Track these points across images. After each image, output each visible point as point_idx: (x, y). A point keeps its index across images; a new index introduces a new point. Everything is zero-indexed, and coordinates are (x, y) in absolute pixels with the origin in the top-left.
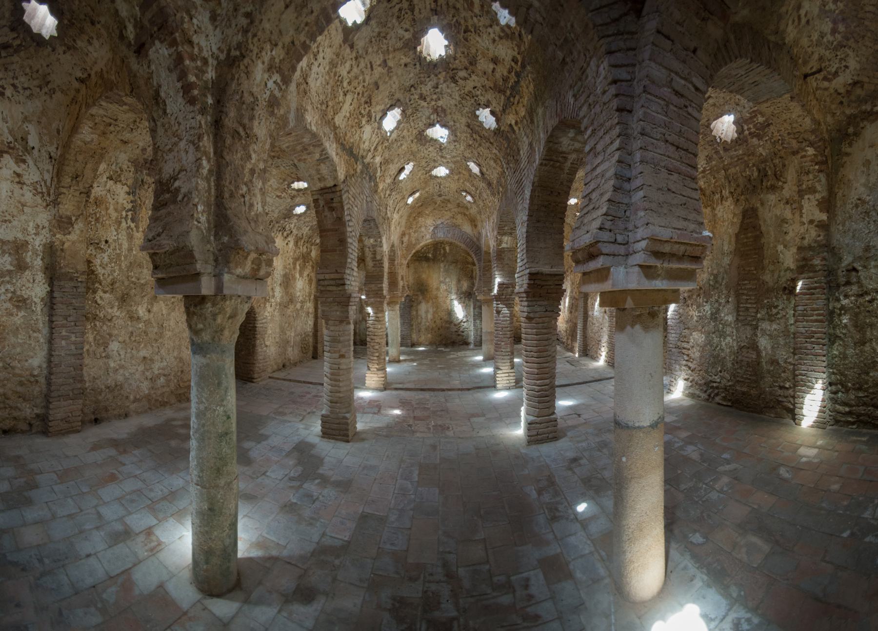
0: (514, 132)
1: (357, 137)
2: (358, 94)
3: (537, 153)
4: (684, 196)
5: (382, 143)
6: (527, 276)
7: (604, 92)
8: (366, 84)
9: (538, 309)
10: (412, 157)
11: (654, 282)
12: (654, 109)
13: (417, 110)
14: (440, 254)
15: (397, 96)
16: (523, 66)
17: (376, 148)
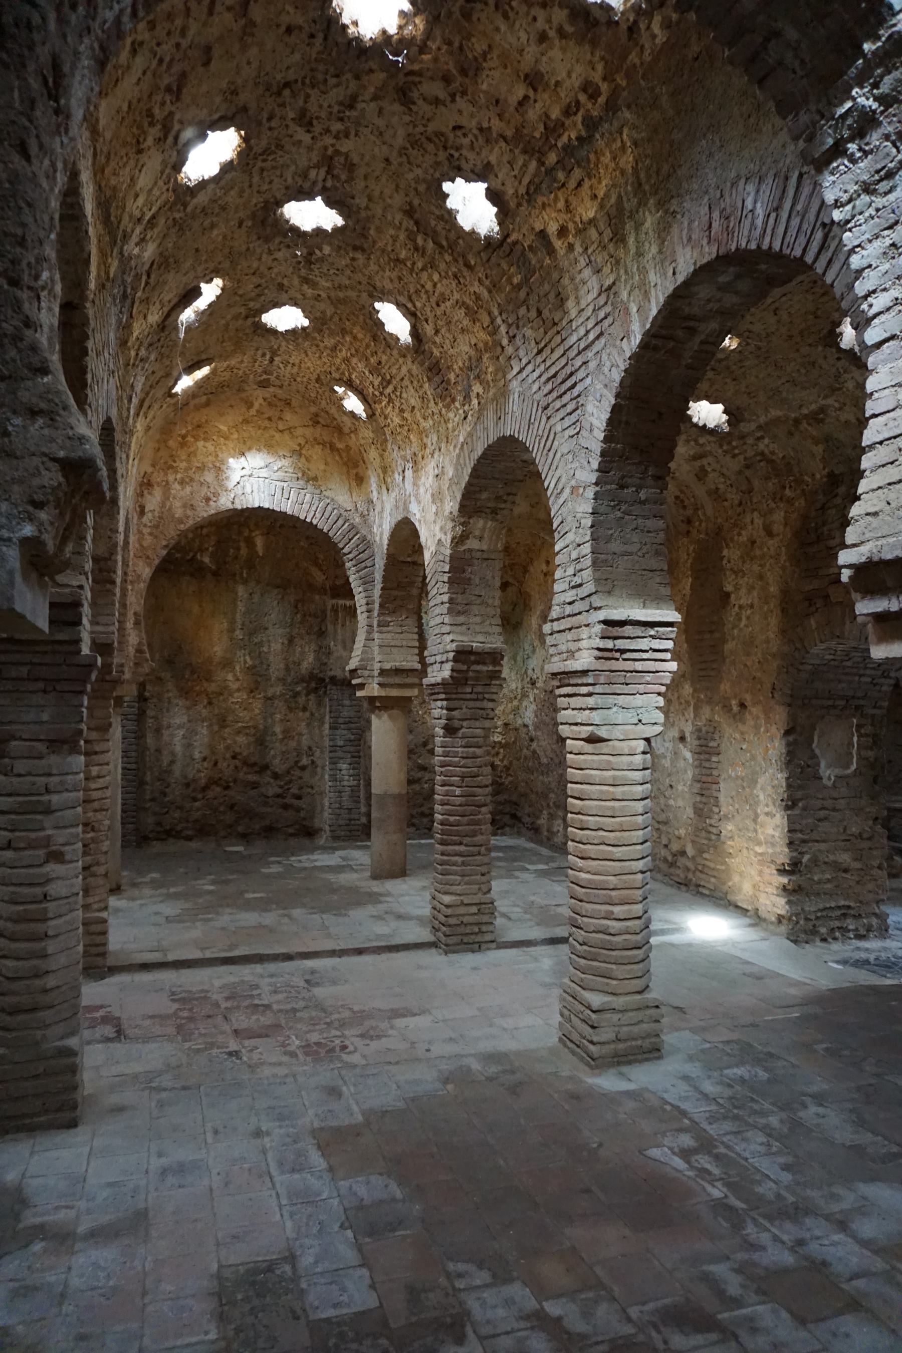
0: (551, 251)
2: (161, 61)
8: (184, 43)
10: (226, 265)
15: (244, 97)
16: (611, 107)
17: (153, 217)
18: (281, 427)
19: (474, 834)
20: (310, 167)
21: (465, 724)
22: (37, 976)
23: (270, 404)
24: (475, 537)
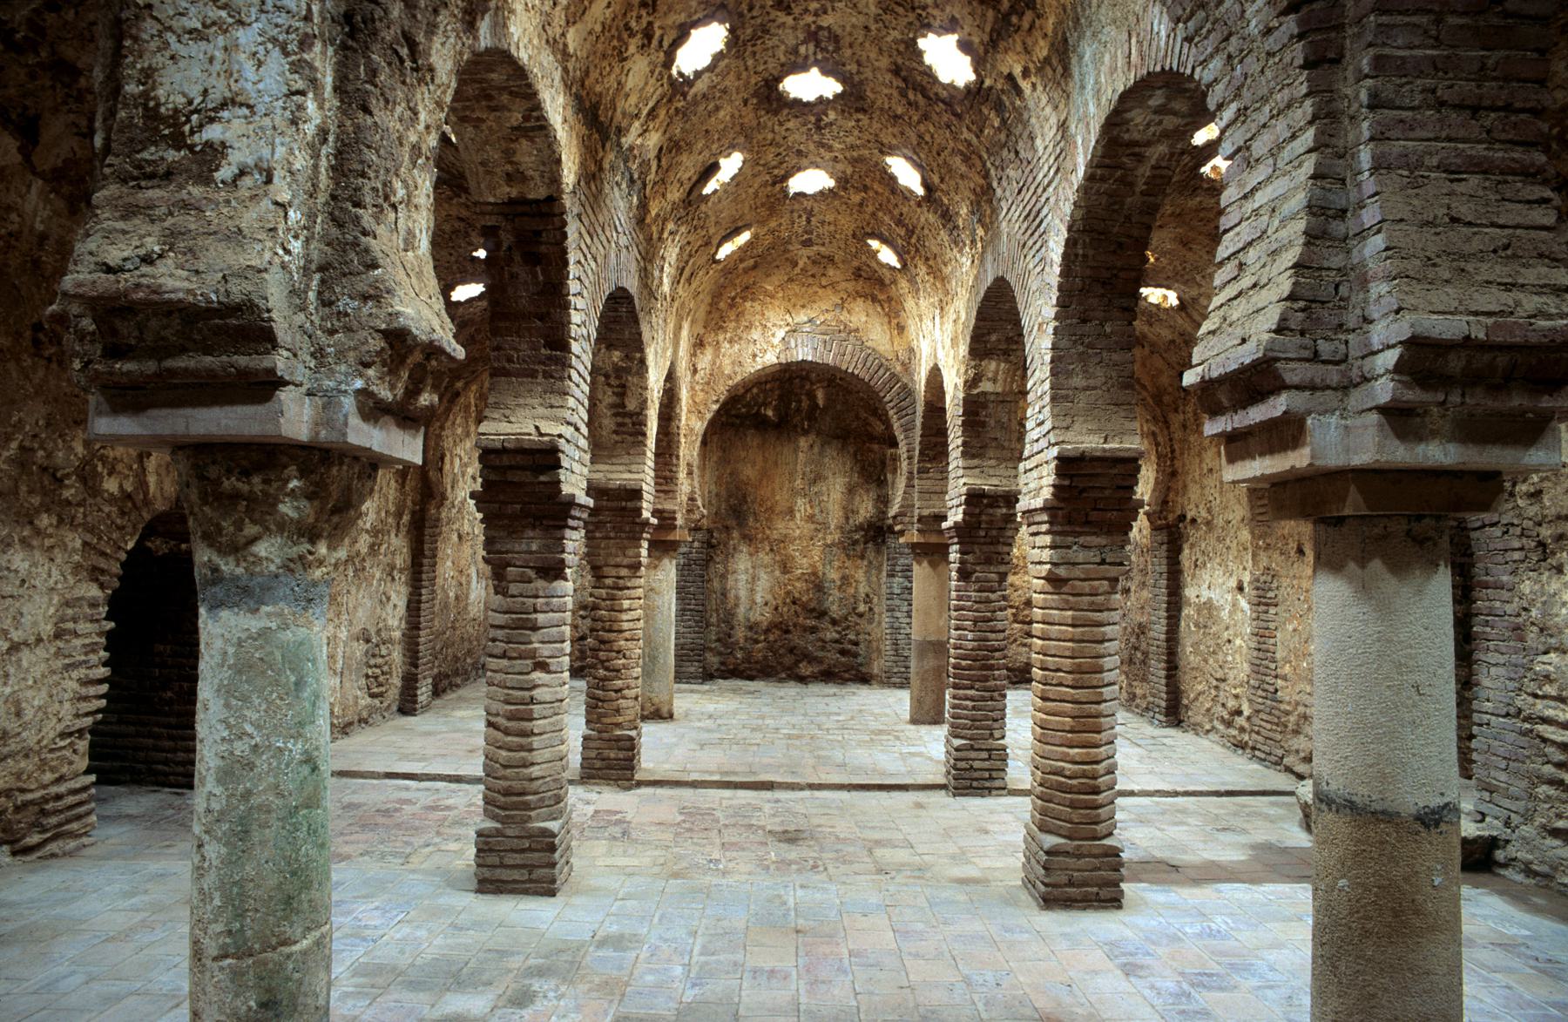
0: (1019, 91)
1: (611, 82)
3: (1080, 150)
4: (1502, 227)
5: (670, 101)
6: (1053, 465)
7: (1268, 31)
9: (1081, 556)
10: (741, 139)
11: (1421, 449)
12: (1400, 42)
13: (768, 32)
14: (798, 410)
17: (653, 109)
18: (824, 283)
19: (986, 679)
20: (798, 45)
21: (978, 568)
22: (525, 766)
23: (814, 262)
24: (989, 379)
